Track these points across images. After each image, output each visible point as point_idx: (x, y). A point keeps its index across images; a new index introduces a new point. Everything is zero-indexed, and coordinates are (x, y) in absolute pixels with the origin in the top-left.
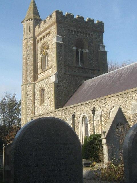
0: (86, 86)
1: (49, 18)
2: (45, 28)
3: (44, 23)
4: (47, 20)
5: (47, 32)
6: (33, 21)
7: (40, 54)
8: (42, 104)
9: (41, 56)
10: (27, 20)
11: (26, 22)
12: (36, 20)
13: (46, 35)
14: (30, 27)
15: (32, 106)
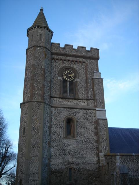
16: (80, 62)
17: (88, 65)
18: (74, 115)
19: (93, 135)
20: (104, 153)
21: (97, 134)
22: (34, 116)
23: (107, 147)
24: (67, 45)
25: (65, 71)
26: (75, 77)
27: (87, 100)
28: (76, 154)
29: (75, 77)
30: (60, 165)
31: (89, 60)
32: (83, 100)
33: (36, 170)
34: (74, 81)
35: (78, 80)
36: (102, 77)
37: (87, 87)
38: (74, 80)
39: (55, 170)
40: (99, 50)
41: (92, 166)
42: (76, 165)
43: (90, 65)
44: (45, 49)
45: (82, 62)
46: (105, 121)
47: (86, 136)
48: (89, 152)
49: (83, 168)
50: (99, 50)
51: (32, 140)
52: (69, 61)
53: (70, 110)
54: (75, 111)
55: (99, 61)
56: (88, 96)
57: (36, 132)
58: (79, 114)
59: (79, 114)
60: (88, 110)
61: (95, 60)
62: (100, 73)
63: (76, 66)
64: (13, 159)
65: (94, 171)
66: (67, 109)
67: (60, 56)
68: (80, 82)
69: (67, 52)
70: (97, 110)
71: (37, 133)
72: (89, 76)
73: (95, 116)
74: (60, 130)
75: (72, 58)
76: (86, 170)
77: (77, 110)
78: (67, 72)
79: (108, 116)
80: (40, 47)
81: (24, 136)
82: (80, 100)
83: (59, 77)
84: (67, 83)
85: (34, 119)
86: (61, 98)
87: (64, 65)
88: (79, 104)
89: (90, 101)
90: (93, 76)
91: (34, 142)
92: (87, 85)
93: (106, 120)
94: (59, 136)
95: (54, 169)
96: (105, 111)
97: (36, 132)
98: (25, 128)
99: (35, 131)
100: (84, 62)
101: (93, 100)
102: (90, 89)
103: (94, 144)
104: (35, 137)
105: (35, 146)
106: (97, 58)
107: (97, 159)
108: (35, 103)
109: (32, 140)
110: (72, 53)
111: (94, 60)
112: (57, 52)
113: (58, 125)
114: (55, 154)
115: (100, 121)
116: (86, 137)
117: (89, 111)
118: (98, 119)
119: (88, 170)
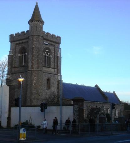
16: (53, 45)
21: (58, 88)
26: (50, 54)
29: (50, 54)
37: (54, 61)
38: (49, 56)
53: (49, 74)
56: (54, 66)
63: (50, 47)
64: (44, 99)
69: (48, 38)
72: (56, 54)
73: (58, 78)
77: (51, 75)
79: (63, 79)
92: (54, 59)
106: (59, 43)
116: (54, 89)
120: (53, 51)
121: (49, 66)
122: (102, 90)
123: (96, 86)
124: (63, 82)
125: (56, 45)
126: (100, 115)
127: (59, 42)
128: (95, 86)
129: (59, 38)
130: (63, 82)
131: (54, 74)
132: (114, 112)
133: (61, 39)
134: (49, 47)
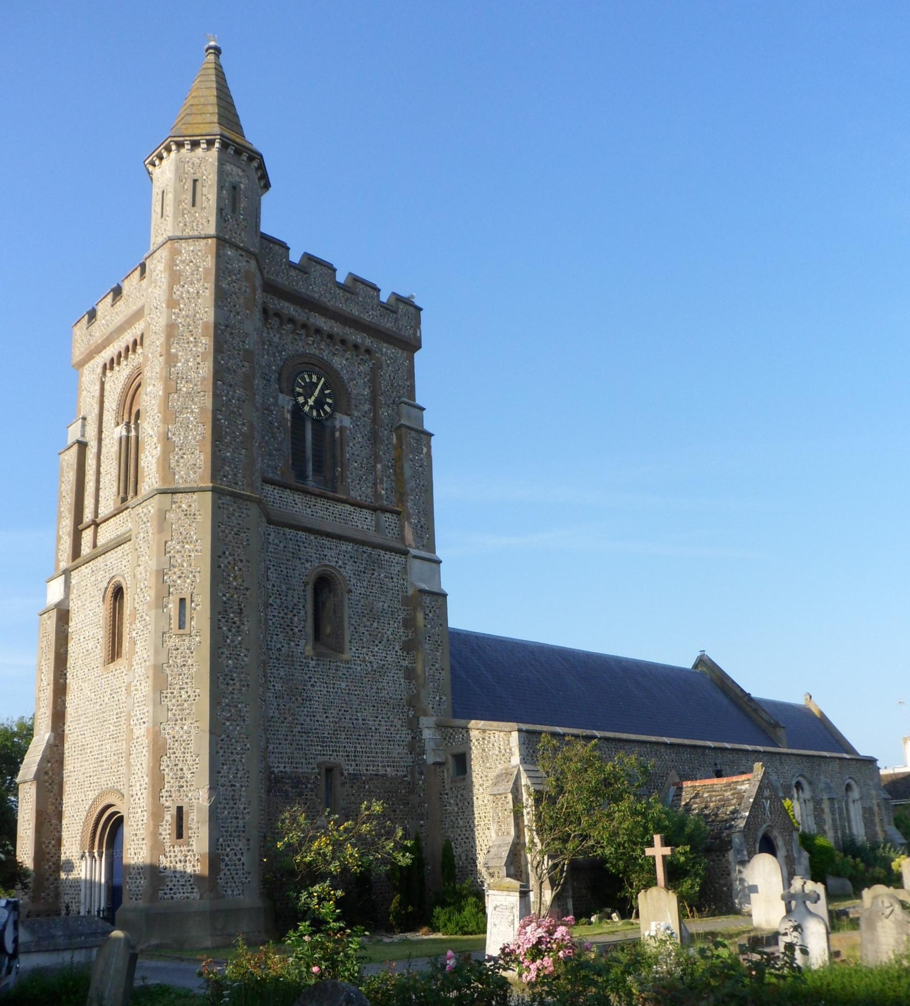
0: (128, 612)
1: (109, 299)
2: (119, 320)
3: (114, 299)
4: (126, 287)
5: (124, 346)
6: (214, 152)
7: (118, 424)
8: (113, 660)
9: (116, 436)
10: (180, 145)
11: (170, 160)
12: (231, 151)
13: (127, 349)
14: (195, 181)
15: (704, 754)
17: (380, 368)
18: (340, 563)
19: (397, 648)
20: (434, 718)
22: (224, 553)
23: (444, 698)
24: (316, 262)
25: (302, 372)
27: (374, 510)
28: (348, 717)
30: (296, 755)
31: (385, 345)
32: (361, 506)
33: (239, 775)
34: (328, 423)
35: (347, 421)
36: (428, 426)
39: (281, 772)
40: (420, 309)
41: (393, 762)
42: (348, 756)
43: (388, 366)
44: (169, 244)
45: (363, 349)
46: (440, 600)
47: (376, 649)
48: (384, 712)
49: (367, 770)
50: (420, 309)
51: (222, 653)
52: (318, 331)
54: (344, 548)
55: (417, 355)
57: (234, 623)
58: (355, 562)
59: (355, 562)
60: (382, 552)
61: (403, 349)
62: (423, 409)
63: (339, 362)
65: (399, 781)
66: (318, 537)
67: (286, 304)
68: (353, 431)
69: (316, 290)
70: (415, 557)
71: (239, 627)
72: (384, 413)
74: (296, 619)
75: (332, 323)
76: (376, 775)
78: (308, 380)
80: (237, 247)
81: (181, 632)
82: (352, 505)
83: (281, 396)
84: (304, 426)
85: (226, 566)
86: (291, 489)
87: (300, 347)
88: (350, 523)
89: (388, 515)
90: (399, 414)
91: (230, 662)
93: (444, 596)
94: (293, 644)
95: (276, 770)
96: (439, 562)
97: (234, 623)
98: (188, 602)
99: (232, 615)
100: (368, 351)
101: (398, 513)
102: (388, 467)
103: (402, 680)
104: (233, 641)
105: (233, 680)
106: (412, 345)
107: (409, 738)
108: (228, 498)
109: (222, 653)
110: (332, 303)
111: (400, 351)
112: (279, 280)
113: (289, 599)
114: (280, 714)
115: (99, 544)
117: (387, 557)
118: (422, 591)
119: (383, 776)
120: (359, 388)
121: (330, 488)
122: (755, 694)
123: (703, 661)
124: (459, 618)
125: (387, 350)
126: (303, 858)
127: (407, 333)
128: (696, 666)
129: (406, 309)
130: (459, 618)
131: (375, 546)
132: (840, 808)
133: (449, 599)
134: (325, 355)
